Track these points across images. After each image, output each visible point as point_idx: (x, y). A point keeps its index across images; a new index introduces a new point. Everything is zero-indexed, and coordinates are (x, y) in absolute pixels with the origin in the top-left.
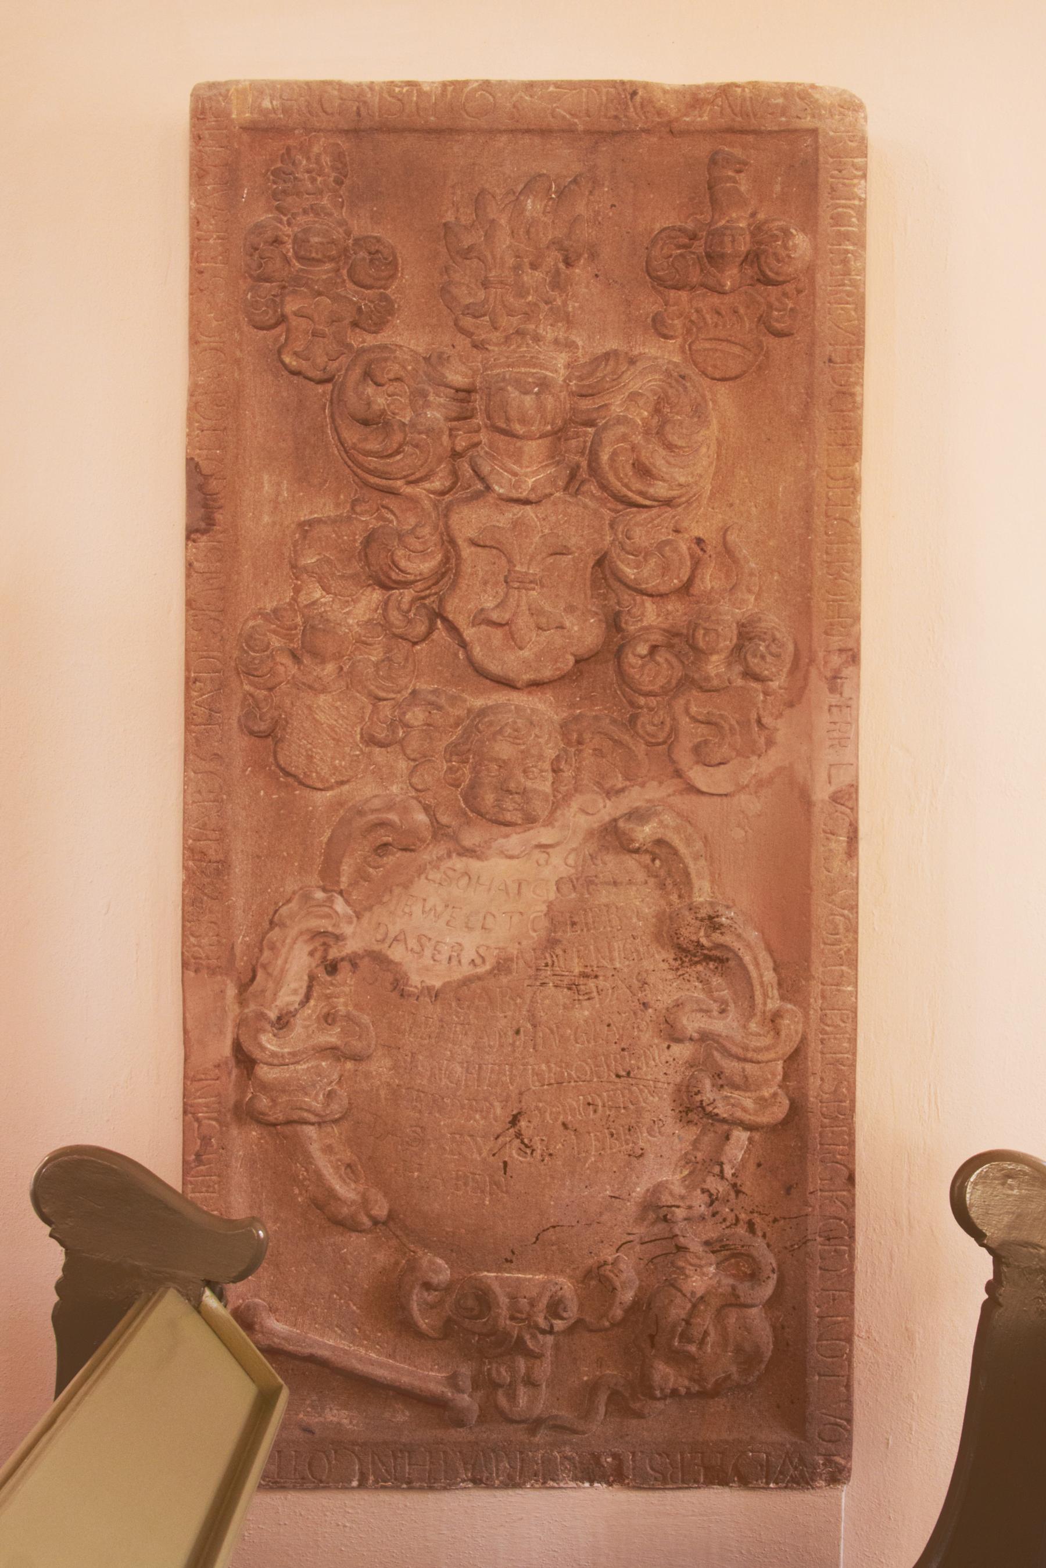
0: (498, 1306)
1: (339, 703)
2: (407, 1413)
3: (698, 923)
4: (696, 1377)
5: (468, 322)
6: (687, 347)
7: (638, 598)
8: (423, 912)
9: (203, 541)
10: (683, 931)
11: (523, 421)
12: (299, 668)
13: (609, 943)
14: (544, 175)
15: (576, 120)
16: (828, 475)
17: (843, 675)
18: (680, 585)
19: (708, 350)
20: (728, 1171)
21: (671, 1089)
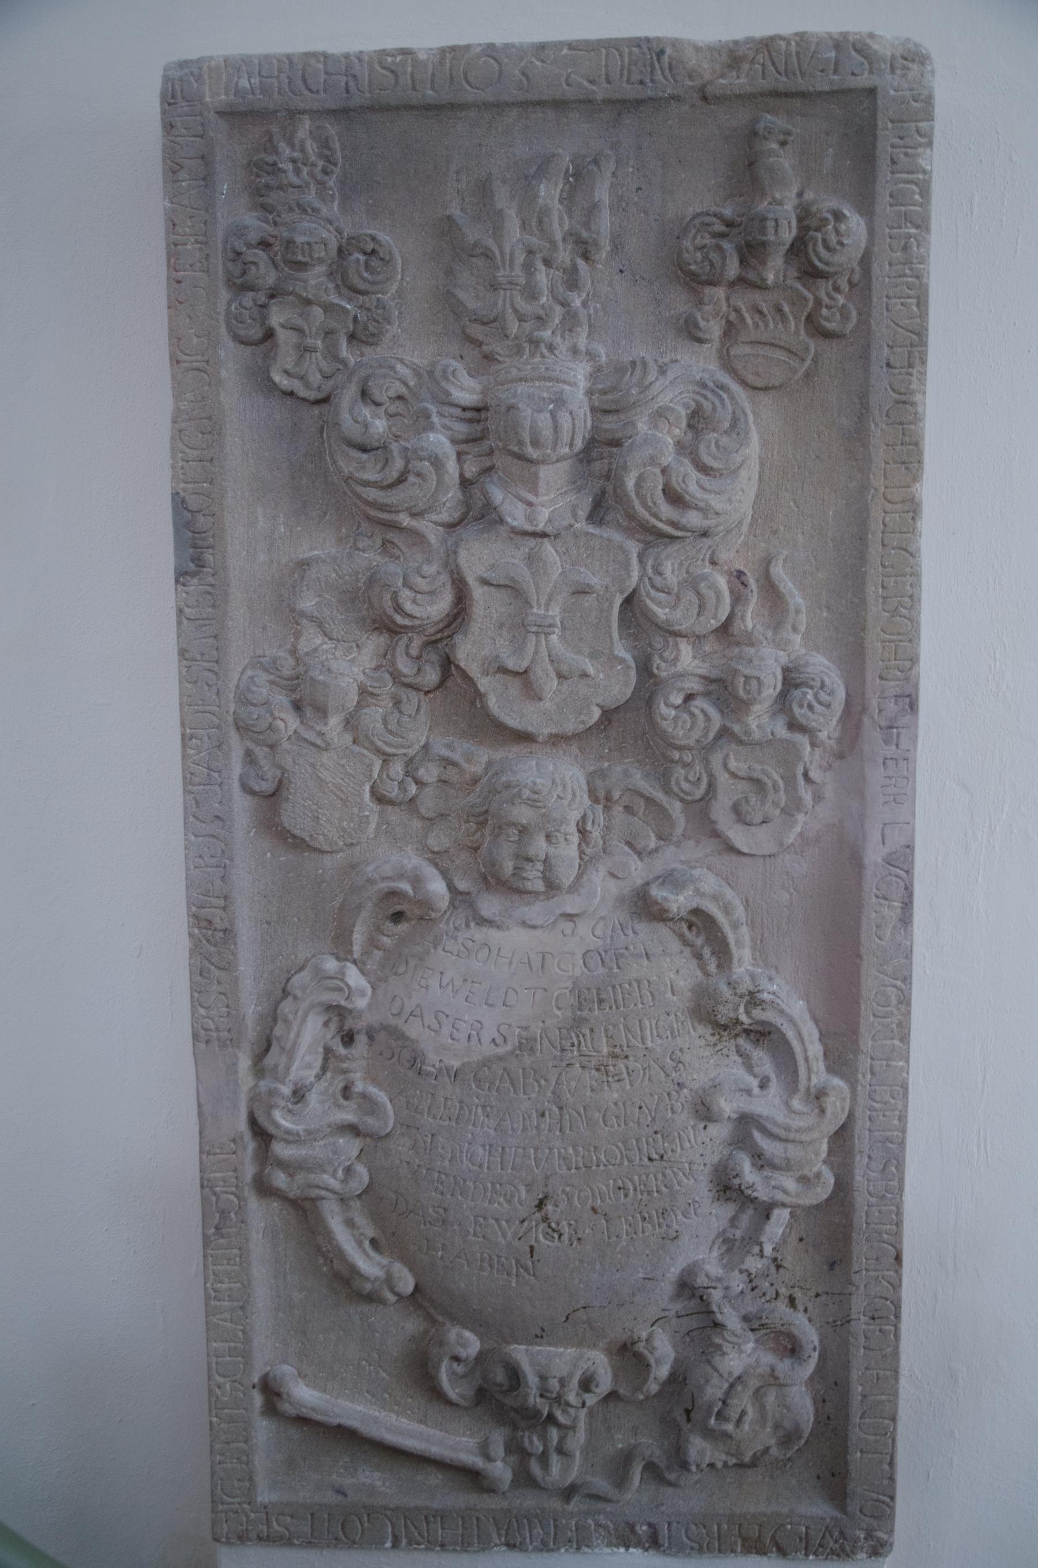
0: (527, 1385)
5: (476, 331)
6: (725, 351)
7: (671, 640)
8: (441, 986)
10: (721, 1008)
13: (640, 1021)
15: (594, 88)
18: (719, 624)
20: (768, 1249)
21: (707, 1170)
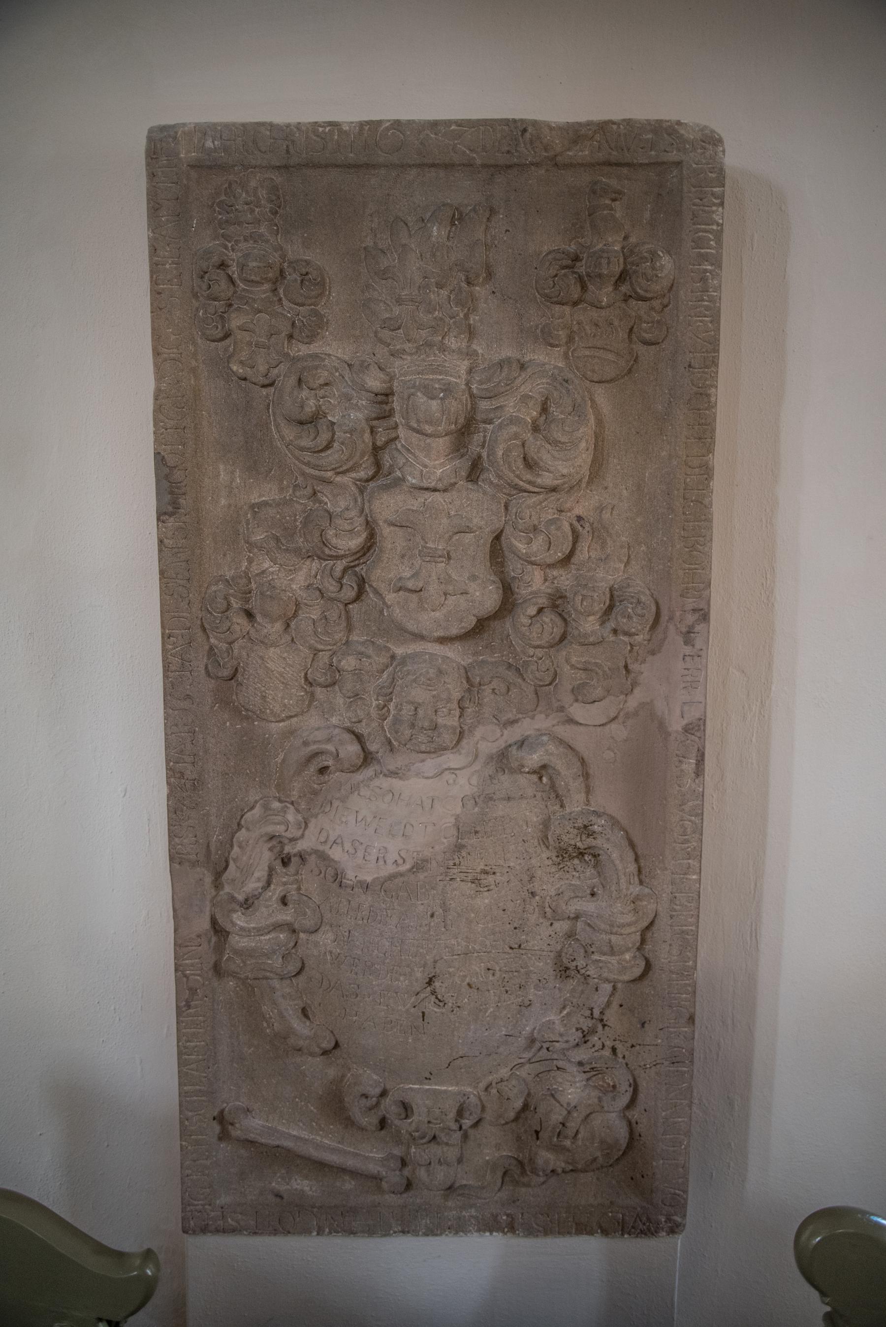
1: (286, 654)
2: (353, 1183)
3: (576, 831)
4: (570, 1161)
5: (386, 334)
9: (171, 522)
11: (430, 423)
12: (253, 626)
14: (448, 204)
15: (475, 155)
16: (686, 464)
17: (696, 630)
19: (587, 356)
